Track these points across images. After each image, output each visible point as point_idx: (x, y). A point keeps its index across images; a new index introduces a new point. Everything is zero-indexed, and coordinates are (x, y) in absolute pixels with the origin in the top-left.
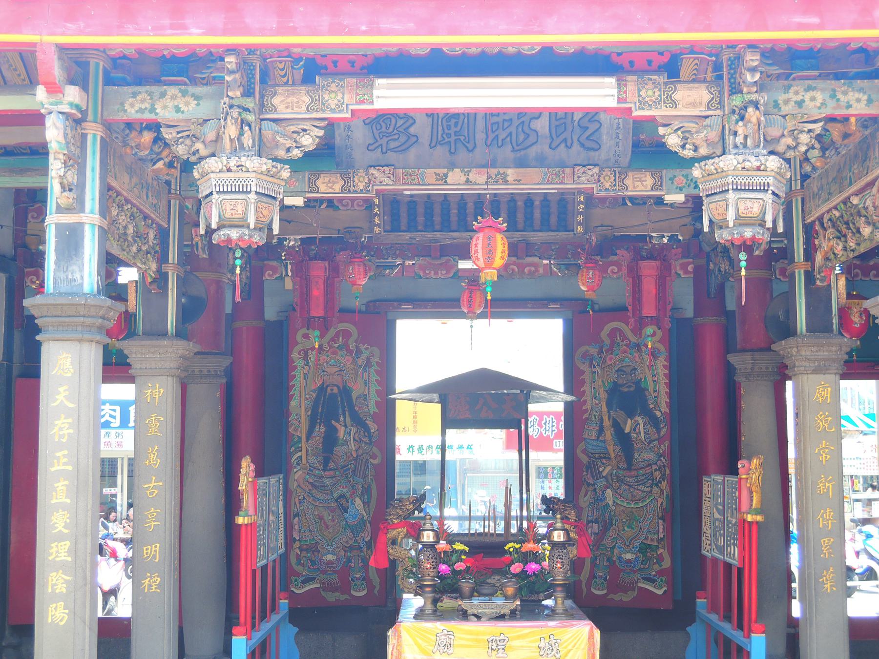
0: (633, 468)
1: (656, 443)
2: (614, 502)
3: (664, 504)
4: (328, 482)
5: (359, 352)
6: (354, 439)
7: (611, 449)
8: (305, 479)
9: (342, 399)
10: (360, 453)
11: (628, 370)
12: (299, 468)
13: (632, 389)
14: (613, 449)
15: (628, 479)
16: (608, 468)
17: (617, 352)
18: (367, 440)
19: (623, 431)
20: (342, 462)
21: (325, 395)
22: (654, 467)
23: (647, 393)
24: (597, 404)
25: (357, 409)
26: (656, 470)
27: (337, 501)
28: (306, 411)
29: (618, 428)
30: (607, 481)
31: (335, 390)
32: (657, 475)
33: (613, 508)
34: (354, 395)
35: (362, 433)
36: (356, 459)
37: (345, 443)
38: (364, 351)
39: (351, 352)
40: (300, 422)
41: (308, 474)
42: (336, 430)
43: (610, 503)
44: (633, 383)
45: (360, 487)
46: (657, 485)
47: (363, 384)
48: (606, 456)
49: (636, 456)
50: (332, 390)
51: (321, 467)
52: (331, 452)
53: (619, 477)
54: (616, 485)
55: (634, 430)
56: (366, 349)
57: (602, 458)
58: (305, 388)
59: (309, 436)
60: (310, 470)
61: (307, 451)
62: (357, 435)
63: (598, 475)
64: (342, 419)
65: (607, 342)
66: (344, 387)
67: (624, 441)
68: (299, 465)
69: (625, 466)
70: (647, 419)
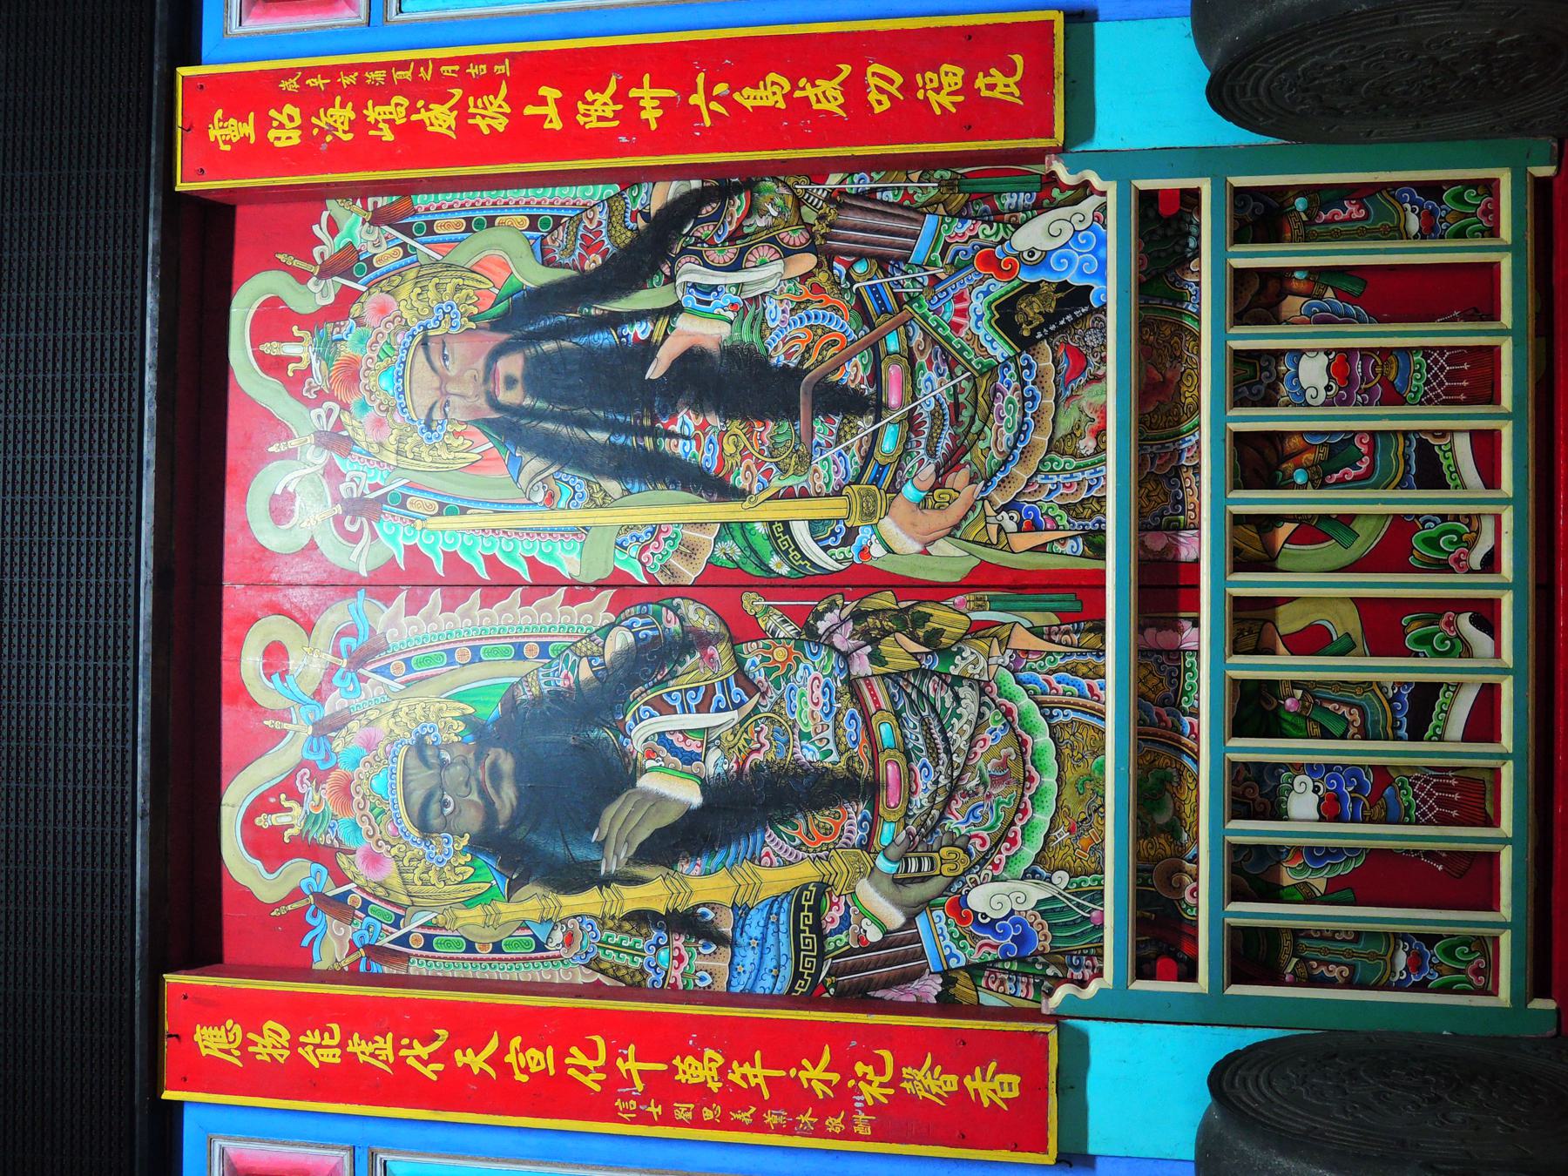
0: (866, 771)
1: (752, 654)
2: (1030, 874)
3: (1039, 619)
4: (934, 387)
5: (347, 263)
6: (736, 266)
7: (777, 879)
8: (922, 505)
9: (555, 333)
10: (796, 237)
11: (423, 779)
12: (865, 535)
13: (507, 764)
14: (774, 869)
15: (921, 799)
16: (865, 890)
17: (344, 831)
18: (739, 204)
19: (691, 815)
20: (844, 325)
21: (532, 413)
22: (862, 666)
23: (524, 695)
24: (569, 940)
25: (594, 262)
26: (876, 658)
27: (1026, 344)
28: (606, 502)
29: (682, 840)
30: (927, 905)
31: (512, 365)
32: (901, 651)
33: (1061, 878)
34: (537, 276)
35: (705, 231)
36: (827, 256)
37: (751, 306)
38: (340, 241)
39: (347, 298)
40: (656, 531)
41: (894, 489)
42: (692, 359)
43: (1035, 893)
44: (479, 757)
45: (962, 228)
46: (947, 654)
47: (484, 237)
48: (808, 907)
49: (809, 754)
50: (510, 382)
51: (865, 424)
52: (795, 375)
53: (911, 847)
54: (950, 861)
55: (689, 758)
56: (333, 229)
57: (817, 928)
58: (499, 507)
59: (717, 487)
60: (878, 479)
61: (789, 494)
62: (715, 256)
63: (901, 950)
64: (640, 330)
65: (301, 873)
66: (498, 324)
67: (742, 807)
68: (852, 533)
69: (855, 812)
70: (641, 697)
